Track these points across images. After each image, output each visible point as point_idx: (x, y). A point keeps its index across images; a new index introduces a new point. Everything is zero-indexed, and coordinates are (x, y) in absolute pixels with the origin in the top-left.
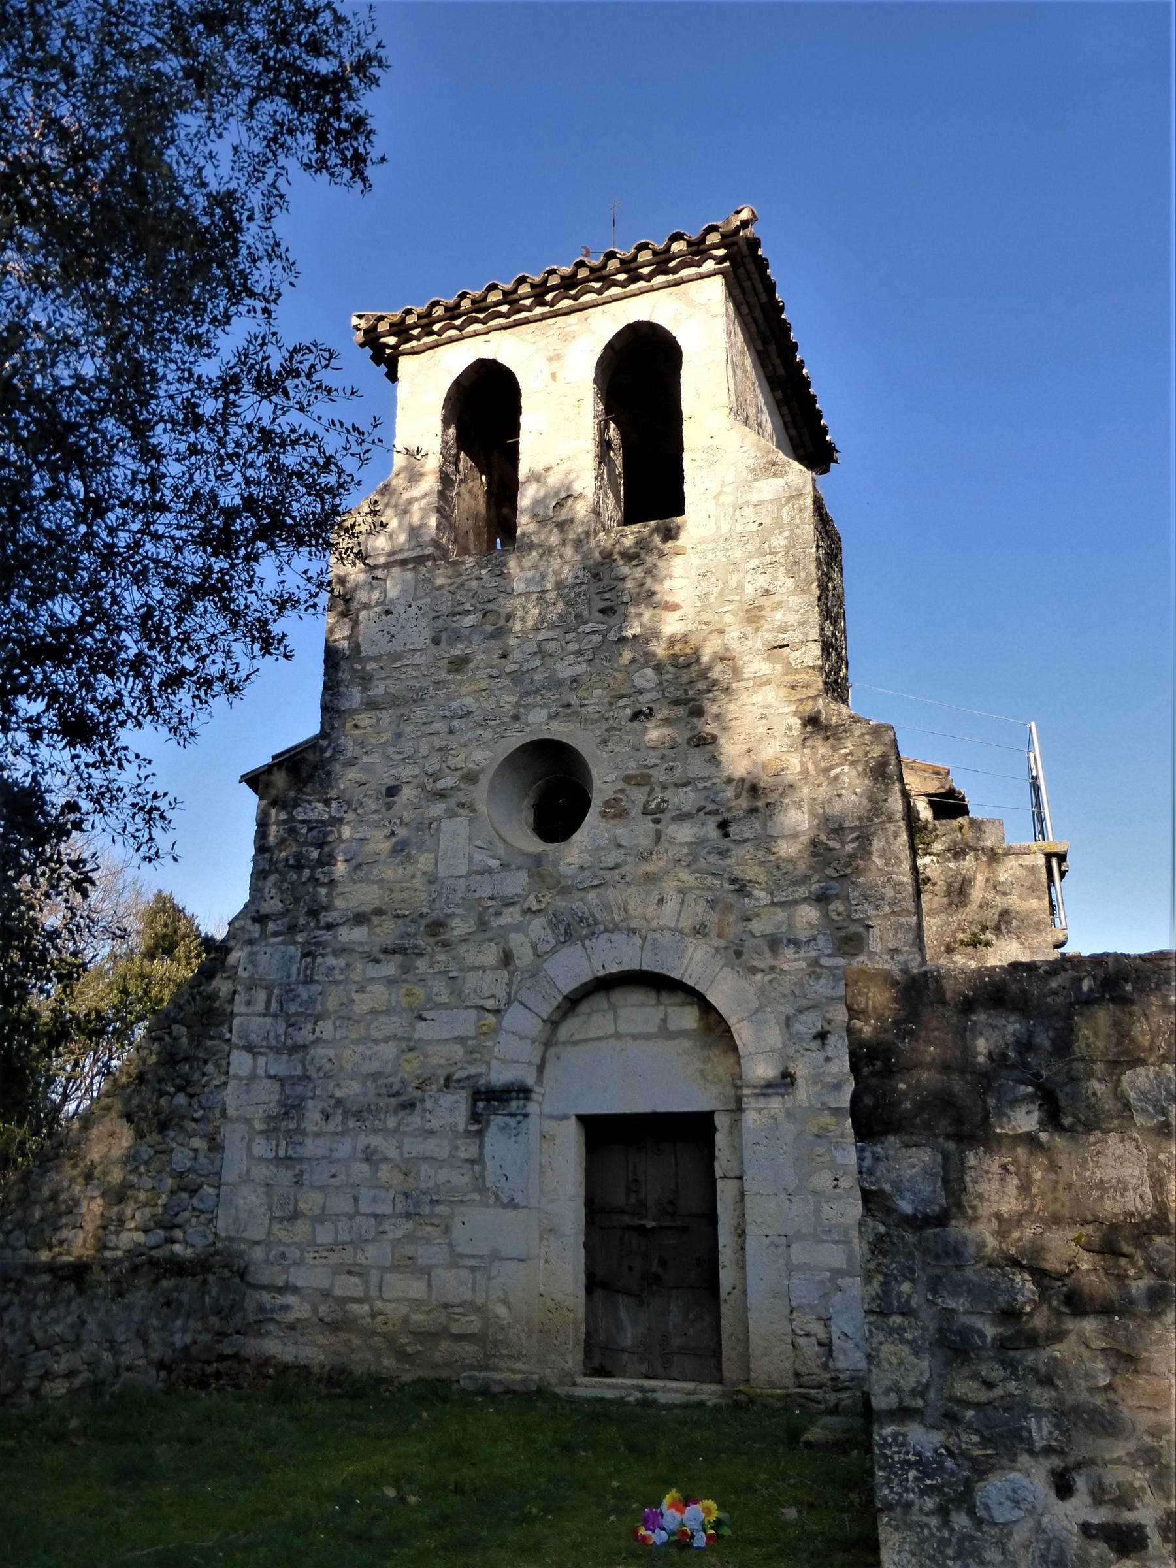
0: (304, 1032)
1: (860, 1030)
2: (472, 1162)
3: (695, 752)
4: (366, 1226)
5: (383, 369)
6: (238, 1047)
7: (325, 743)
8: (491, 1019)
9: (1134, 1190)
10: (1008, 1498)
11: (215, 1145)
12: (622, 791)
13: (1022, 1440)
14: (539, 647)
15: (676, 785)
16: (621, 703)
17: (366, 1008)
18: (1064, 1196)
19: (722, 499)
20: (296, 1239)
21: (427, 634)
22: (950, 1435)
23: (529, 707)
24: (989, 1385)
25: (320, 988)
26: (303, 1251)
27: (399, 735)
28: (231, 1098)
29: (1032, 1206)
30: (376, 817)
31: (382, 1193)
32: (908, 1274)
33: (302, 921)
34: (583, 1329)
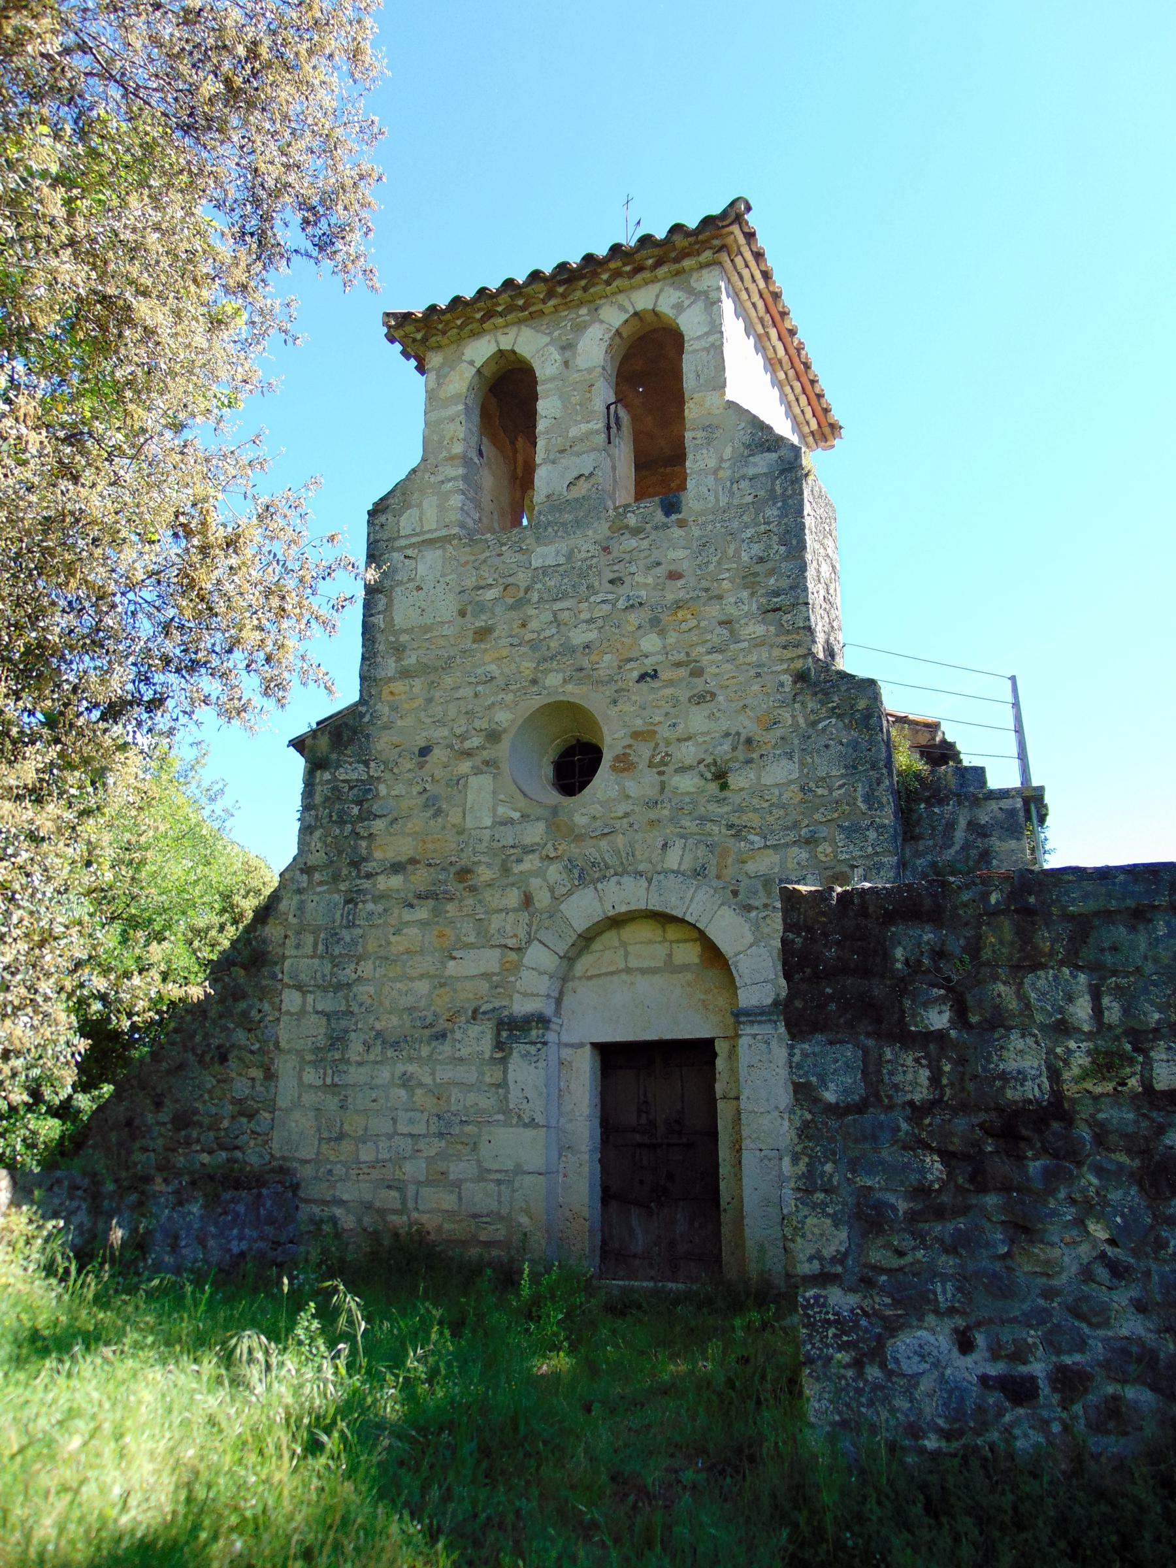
0: (348, 971)
1: (793, 941)
2: (498, 1086)
3: (695, 709)
4: (406, 1145)
5: (413, 363)
6: (289, 987)
7: (363, 709)
8: (513, 956)
9: (1033, 1080)
10: (915, 1353)
11: (270, 1076)
12: (630, 746)
13: (929, 1301)
14: (555, 616)
15: (678, 740)
16: (628, 666)
17: (401, 949)
18: (970, 1086)
19: (721, 474)
20: (342, 1158)
21: (454, 608)
22: (865, 1297)
23: (546, 672)
24: (901, 1254)
25: (360, 931)
26: (348, 1169)
27: (429, 700)
28: (285, 1033)
29: (942, 1095)
30: (410, 775)
31: (418, 1114)
32: (830, 1155)
33: (345, 872)
34: (599, 1236)
